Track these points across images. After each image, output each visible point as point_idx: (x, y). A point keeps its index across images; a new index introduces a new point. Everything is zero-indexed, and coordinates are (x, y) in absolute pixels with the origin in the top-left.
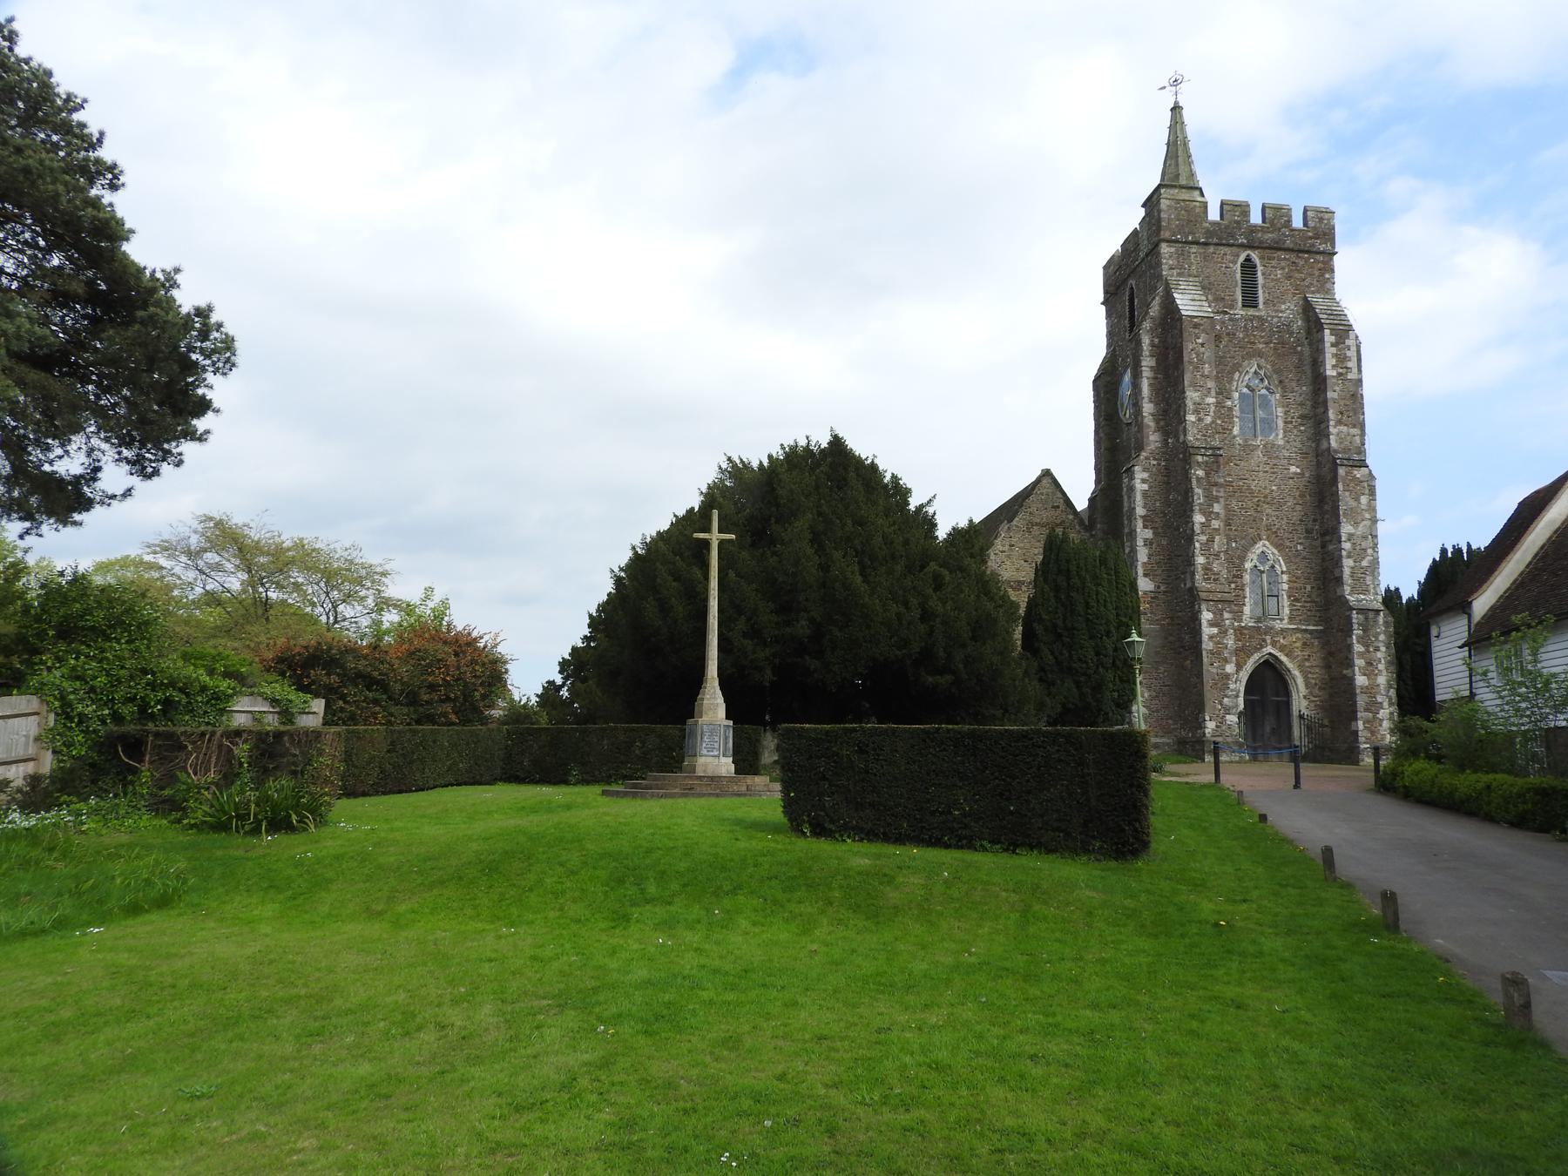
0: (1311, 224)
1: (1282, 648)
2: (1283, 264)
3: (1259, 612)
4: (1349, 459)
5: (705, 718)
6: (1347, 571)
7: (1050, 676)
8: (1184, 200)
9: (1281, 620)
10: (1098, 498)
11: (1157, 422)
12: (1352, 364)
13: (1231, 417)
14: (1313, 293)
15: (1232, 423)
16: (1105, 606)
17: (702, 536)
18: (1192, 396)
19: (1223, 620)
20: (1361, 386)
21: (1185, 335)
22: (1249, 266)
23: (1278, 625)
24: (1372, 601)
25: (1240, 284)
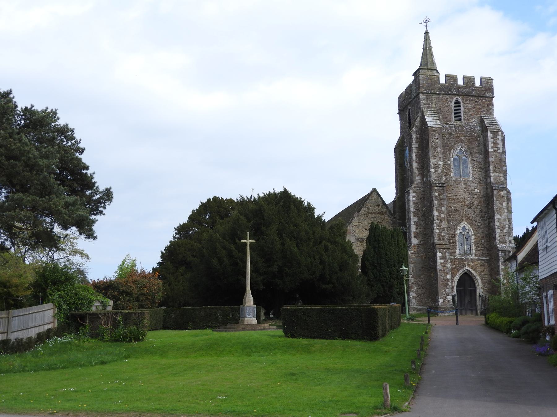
0: (483, 85)
1: (472, 268)
2: (472, 102)
3: (462, 252)
4: (498, 187)
5: (247, 304)
6: (497, 235)
7: (372, 283)
8: (429, 75)
9: (472, 255)
10: (397, 201)
11: (419, 171)
12: (500, 146)
13: (450, 169)
14: (485, 114)
15: (451, 171)
16: (393, 255)
17: (244, 241)
18: (433, 161)
19: (446, 256)
20: (505, 154)
21: (430, 135)
22: (457, 103)
23: (470, 257)
24: (507, 247)
25: (453, 111)
